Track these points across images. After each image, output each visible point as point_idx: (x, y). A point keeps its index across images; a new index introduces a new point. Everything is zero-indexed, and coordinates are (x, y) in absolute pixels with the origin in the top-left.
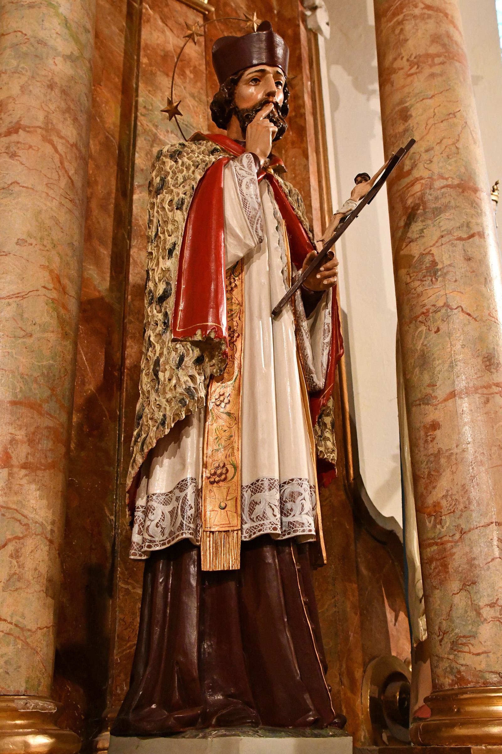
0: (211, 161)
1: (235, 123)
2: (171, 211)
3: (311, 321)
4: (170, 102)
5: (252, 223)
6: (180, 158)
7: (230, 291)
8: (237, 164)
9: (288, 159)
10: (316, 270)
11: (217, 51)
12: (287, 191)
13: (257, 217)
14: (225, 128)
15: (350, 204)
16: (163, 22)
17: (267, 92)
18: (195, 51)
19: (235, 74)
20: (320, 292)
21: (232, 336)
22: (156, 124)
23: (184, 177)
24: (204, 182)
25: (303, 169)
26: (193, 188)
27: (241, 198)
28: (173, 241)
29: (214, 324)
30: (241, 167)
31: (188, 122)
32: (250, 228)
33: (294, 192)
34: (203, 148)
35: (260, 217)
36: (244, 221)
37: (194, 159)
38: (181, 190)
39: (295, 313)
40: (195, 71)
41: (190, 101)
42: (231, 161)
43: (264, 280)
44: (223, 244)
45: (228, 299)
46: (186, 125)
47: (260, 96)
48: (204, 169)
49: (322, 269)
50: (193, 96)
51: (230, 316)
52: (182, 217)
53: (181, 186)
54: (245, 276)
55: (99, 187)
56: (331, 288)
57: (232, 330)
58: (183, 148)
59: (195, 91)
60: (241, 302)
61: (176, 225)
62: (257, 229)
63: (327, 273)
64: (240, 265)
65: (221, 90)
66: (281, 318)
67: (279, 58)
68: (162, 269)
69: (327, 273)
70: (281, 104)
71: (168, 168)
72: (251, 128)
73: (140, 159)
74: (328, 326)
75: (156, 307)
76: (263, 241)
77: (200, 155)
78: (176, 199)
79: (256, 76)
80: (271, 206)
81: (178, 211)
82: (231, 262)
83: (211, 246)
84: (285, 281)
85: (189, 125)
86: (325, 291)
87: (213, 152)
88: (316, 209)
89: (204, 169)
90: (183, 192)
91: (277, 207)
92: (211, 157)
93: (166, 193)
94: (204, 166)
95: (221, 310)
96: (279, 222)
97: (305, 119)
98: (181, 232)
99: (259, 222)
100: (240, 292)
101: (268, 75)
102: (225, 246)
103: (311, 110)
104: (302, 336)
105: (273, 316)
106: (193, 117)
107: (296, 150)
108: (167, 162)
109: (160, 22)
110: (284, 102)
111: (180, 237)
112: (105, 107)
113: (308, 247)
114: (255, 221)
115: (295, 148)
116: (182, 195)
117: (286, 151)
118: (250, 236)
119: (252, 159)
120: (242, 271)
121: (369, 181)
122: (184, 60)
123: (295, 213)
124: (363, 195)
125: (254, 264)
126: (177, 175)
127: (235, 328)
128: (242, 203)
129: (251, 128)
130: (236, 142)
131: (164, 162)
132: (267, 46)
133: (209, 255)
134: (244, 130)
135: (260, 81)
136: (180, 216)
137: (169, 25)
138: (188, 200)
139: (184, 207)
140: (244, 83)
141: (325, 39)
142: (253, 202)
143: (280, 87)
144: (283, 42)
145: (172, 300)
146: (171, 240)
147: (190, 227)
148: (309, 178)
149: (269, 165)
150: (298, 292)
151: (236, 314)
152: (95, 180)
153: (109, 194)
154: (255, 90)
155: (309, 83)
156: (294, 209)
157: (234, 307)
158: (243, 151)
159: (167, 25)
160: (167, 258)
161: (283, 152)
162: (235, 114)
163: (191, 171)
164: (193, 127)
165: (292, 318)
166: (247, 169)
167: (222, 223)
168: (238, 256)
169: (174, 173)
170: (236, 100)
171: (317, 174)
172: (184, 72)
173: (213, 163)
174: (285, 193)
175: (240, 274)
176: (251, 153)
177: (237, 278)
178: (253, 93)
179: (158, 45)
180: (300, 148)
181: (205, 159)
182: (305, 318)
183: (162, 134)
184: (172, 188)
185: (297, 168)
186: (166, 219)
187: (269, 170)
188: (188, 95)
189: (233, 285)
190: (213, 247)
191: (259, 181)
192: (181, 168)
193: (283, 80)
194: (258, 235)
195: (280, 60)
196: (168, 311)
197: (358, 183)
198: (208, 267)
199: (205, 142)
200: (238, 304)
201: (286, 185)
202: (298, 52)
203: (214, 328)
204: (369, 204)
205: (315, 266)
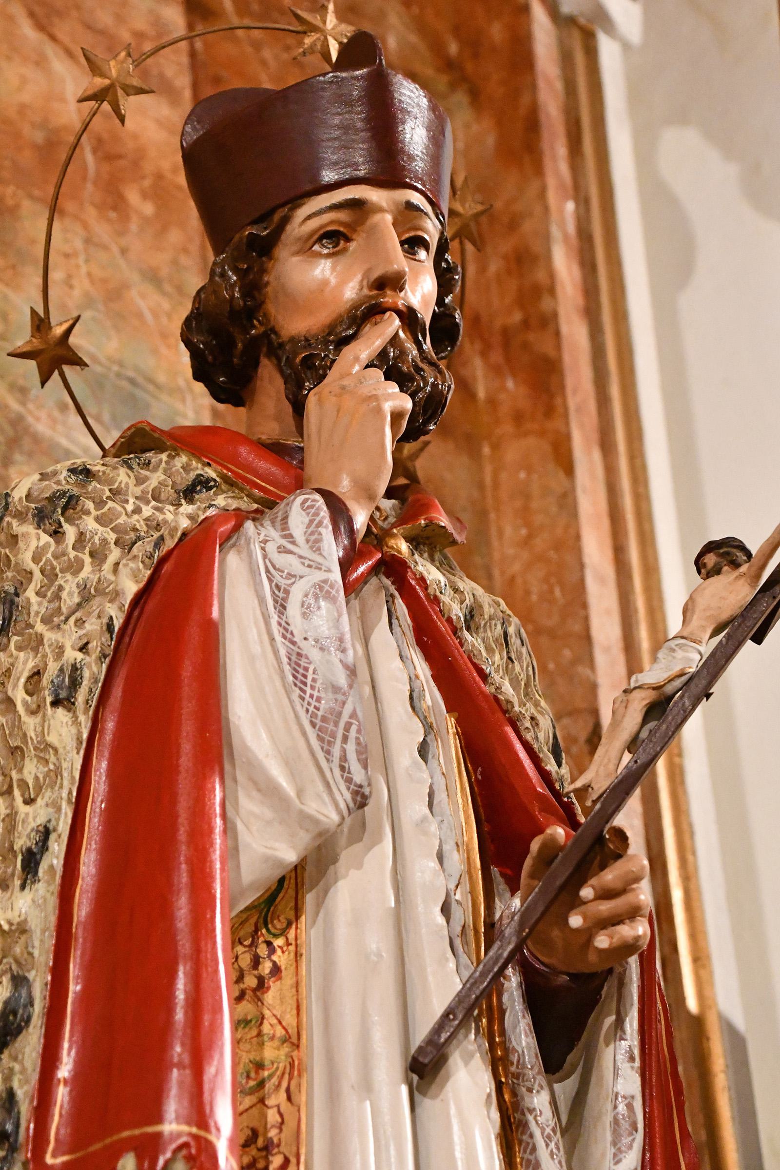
0: (176, 529)
1: (270, 383)
2: (33, 713)
3: (566, 1088)
4: (40, 324)
5: (326, 741)
7: (254, 990)
8: (269, 531)
9: (504, 476)
10: (566, 896)
11: (196, 143)
12: (457, 611)
14: (238, 402)
15: (679, 654)
16: (41, 27)
17: (376, 274)
18: (159, 122)
19: (263, 218)
20: (592, 976)
22: (21, 382)
23: (83, 588)
24: (152, 604)
25: (554, 509)
26: (110, 627)
27: (283, 652)
28: (41, 820)
29: (185, 1128)
30: (284, 542)
31: (137, 369)
32: (321, 756)
33: (488, 610)
34: (155, 478)
35: (354, 715)
36: (297, 734)
37: (122, 519)
38: (70, 637)
39: (500, 1061)
40: (158, 192)
41: (143, 296)
42: (249, 525)
43: (378, 941)
44: (218, 821)
45: (239, 1024)
46: (132, 381)
47: (351, 291)
48: (151, 557)
49: (586, 892)
50: (153, 277)
51: (253, 1085)
52: (74, 731)
53: (72, 620)
54: (309, 931)
56: (633, 962)
57: (260, 1142)
58: (83, 485)
59: (161, 260)
60: (293, 1031)
62: (344, 758)
63: (605, 907)
64: (291, 892)
65: (215, 274)
66: (442, 1086)
67: (411, 158)
69: (605, 907)
70: (426, 315)
71: (26, 558)
72: (320, 402)
74: (630, 1106)
76: (371, 802)
77: (150, 504)
78: (53, 668)
79: (332, 222)
80: (399, 667)
81: (60, 711)
82: (252, 886)
83: (174, 828)
84: (458, 942)
85: (140, 380)
86: (610, 971)
87: (189, 493)
88: (607, 650)
89: (151, 557)
90: (73, 639)
91: (423, 669)
92: (187, 508)
93: (19, 648)
94: (150, 548)
95: (210, 1071)
96: (428, 728)
97: (557, 334)
98: (69, 786)
100: (290, 993)
101: (377, 218)
102: (229, 829)
103: (580, 301)
104: (534, 1149)
105: (415, 1078)
106: (155, 351)
107: (531, 441)
108: (25, 535)
109: (27, 30)
110: (440, 302)
111: (64, 805)
113: (541, 810)
114: (337, 729)
115: (526, 434)
116: (72, 655)
117: (496, 447)
118: (321, 787)
119: (324, 512)
120: (298, 911)
121: (744, 568)
122: (120, 157)
123: (489, 690)
124: (725, 616)
125: (341, 884)
126: (60, 581)
127: (273, 1133)
128: (287, 668)
129: (320, 402)
130: (277, 450)
131: (15, 538)
132: (367, 120)
133: (165, 861)
134: (299, 407)
135: (348, 240)
136: (65, 730)
137: (60, 35)
138: (93, 670)
139: (81, 697)
140: (295, 248)
141: (626, 46)
142: (329, 668)
143: (422, 254)
144: (424, 102)
146: (33, 817)
147: (101, 768)
148: (578, 537)
149: (394, 526)
150: (513, 980)
151: (275, 1080)
154: (333, 269)
155: (570, 206)
156: (484, 677)
157: (269, 1053)
158: (299, 484)
159: (53, 38)
160: (17, 883)
161: (486, 450)
162: (268, 356)
163: (108, 566)
164: (158, 386)
165: (487, 1083)
166: (303, 549)
167: (215, 746)
168: (279, 863)
169: (50, 575)
170: (271, 308)
171: (606, 523)
172: (121, 197)
173: (184, 534)
174: (449, 620)
175: (289, 924)
176: (319, 491)
177: (278, 942)
178: (325, 283)
179: (23, 109)
180: (542, 434)
181: (161, 517)
182: (541, 1079)
183: (43, 414)
184: (40, 628)
185: (535, 505)
186: (18, 743)
187: (392, 542)
188: (135, 277)
190: (182, 834)
191: (350, 589)
192: (72, 554)
193: (431, 229)
194: (349, 781)
195: (419, 165)
196: (16, 1085)
197: (708, 576)
198: (166, 911)
199: (164, 457)
200: (286, 1039)
201: (456, 590)
202: (525, 100)
203: (185, 1145)
204: (758, 639)
205: (559, 882)
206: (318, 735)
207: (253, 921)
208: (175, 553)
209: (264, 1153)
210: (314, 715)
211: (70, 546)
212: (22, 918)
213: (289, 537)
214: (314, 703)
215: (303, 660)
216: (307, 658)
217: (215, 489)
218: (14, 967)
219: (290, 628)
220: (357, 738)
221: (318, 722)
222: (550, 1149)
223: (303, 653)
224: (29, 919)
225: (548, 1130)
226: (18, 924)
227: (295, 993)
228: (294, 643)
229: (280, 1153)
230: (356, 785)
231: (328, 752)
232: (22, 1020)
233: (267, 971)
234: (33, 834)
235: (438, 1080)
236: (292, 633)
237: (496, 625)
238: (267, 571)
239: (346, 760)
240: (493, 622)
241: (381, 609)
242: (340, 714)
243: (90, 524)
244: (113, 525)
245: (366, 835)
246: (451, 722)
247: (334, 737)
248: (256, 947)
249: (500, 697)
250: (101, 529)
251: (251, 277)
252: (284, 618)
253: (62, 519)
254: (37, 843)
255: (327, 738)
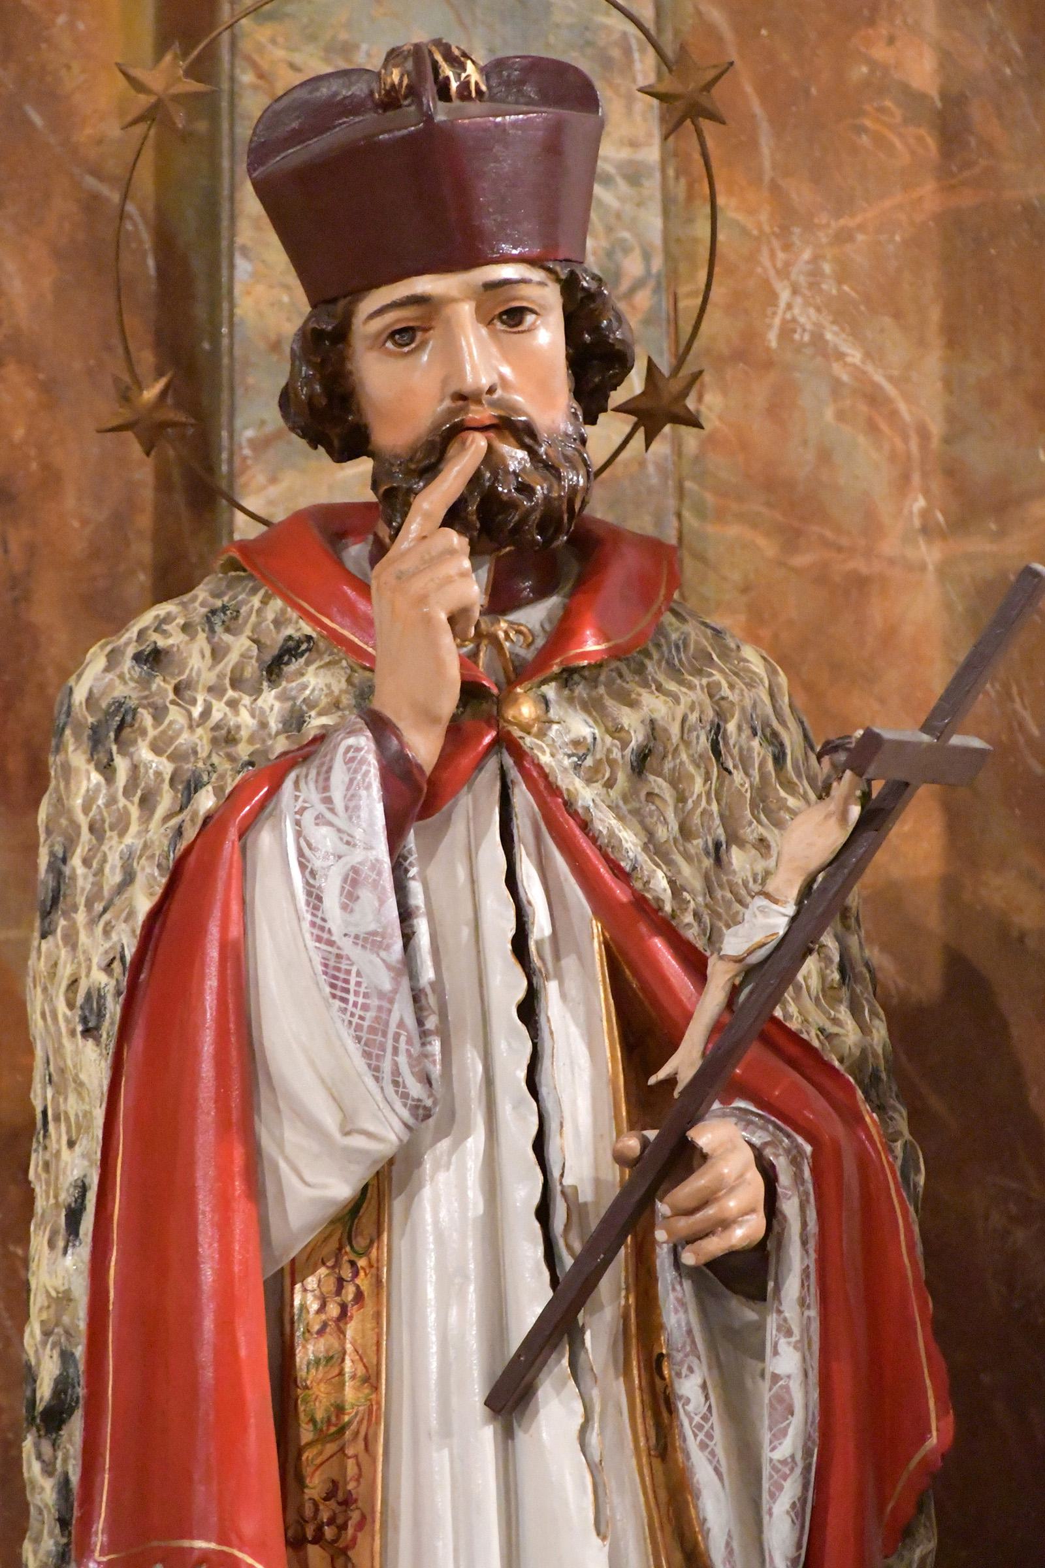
6: (123, 751)
13: (393, 1028)
21: (340, 1521)
35: (401, 1024)
55: (70, 502)
57: (340, 1496)
61: (466, 932)
62: (396, 1072)
64: (374, 1202)
68: (47, 1292)
69: (684, 1224)
73: (260, 289)
75: (37, 1446)
79: (398, 321)
99: (403, 1046)
112: (71, 25)
127: (351, 1486)
145: (75, 1426)
152: (46, 466)
153: (119, 522)
181: (232, 721)
189: (349, 1292)
194: (405, 1096)
206: (364, 1051)
207: (336, 1237)
208: (196, 848)
209: (344, 1507)
210: (359, 1028)
211: (121, 790)
212: (66, 1287)
213: (328, 801)
214: (358, 1012)
215: (344, 961)
216: (348, 959)
217: (306, 655)
218: (63, 1340)
219: (327, 926)
220: (407, 1050)
221: (364, 1035)
222: (699, 1439)
223: (344, 953)
224: (73, 1288)
225: (697, 1419)
226: (64, 1292)
227: (374, 1325)
228: (331, 943)
229: (358, 1508)
230: (413, 1100)
231: (377, 1069)
232: (72, 1400)
233: (350, 1297)
234: (72, 1190)
235: (528, 1413)
236: (330, 931)
237: (698, 737)
238: (301, 854)
239: (399, 1074)
240: (695, 734)
241: (492, 810)
242: (387, 1023)
243: (144, 753)
244: (169, 751)
245: (455, 1127)
246: (597, 927)
247: (384, 1050)
248: (340, 1268)
249: (648, 896)
250: (156, 759)
251: (330, 369)
252: (320, 914)
253: (114, 748)
254: (76, 1201)
255: (375, 1051)
